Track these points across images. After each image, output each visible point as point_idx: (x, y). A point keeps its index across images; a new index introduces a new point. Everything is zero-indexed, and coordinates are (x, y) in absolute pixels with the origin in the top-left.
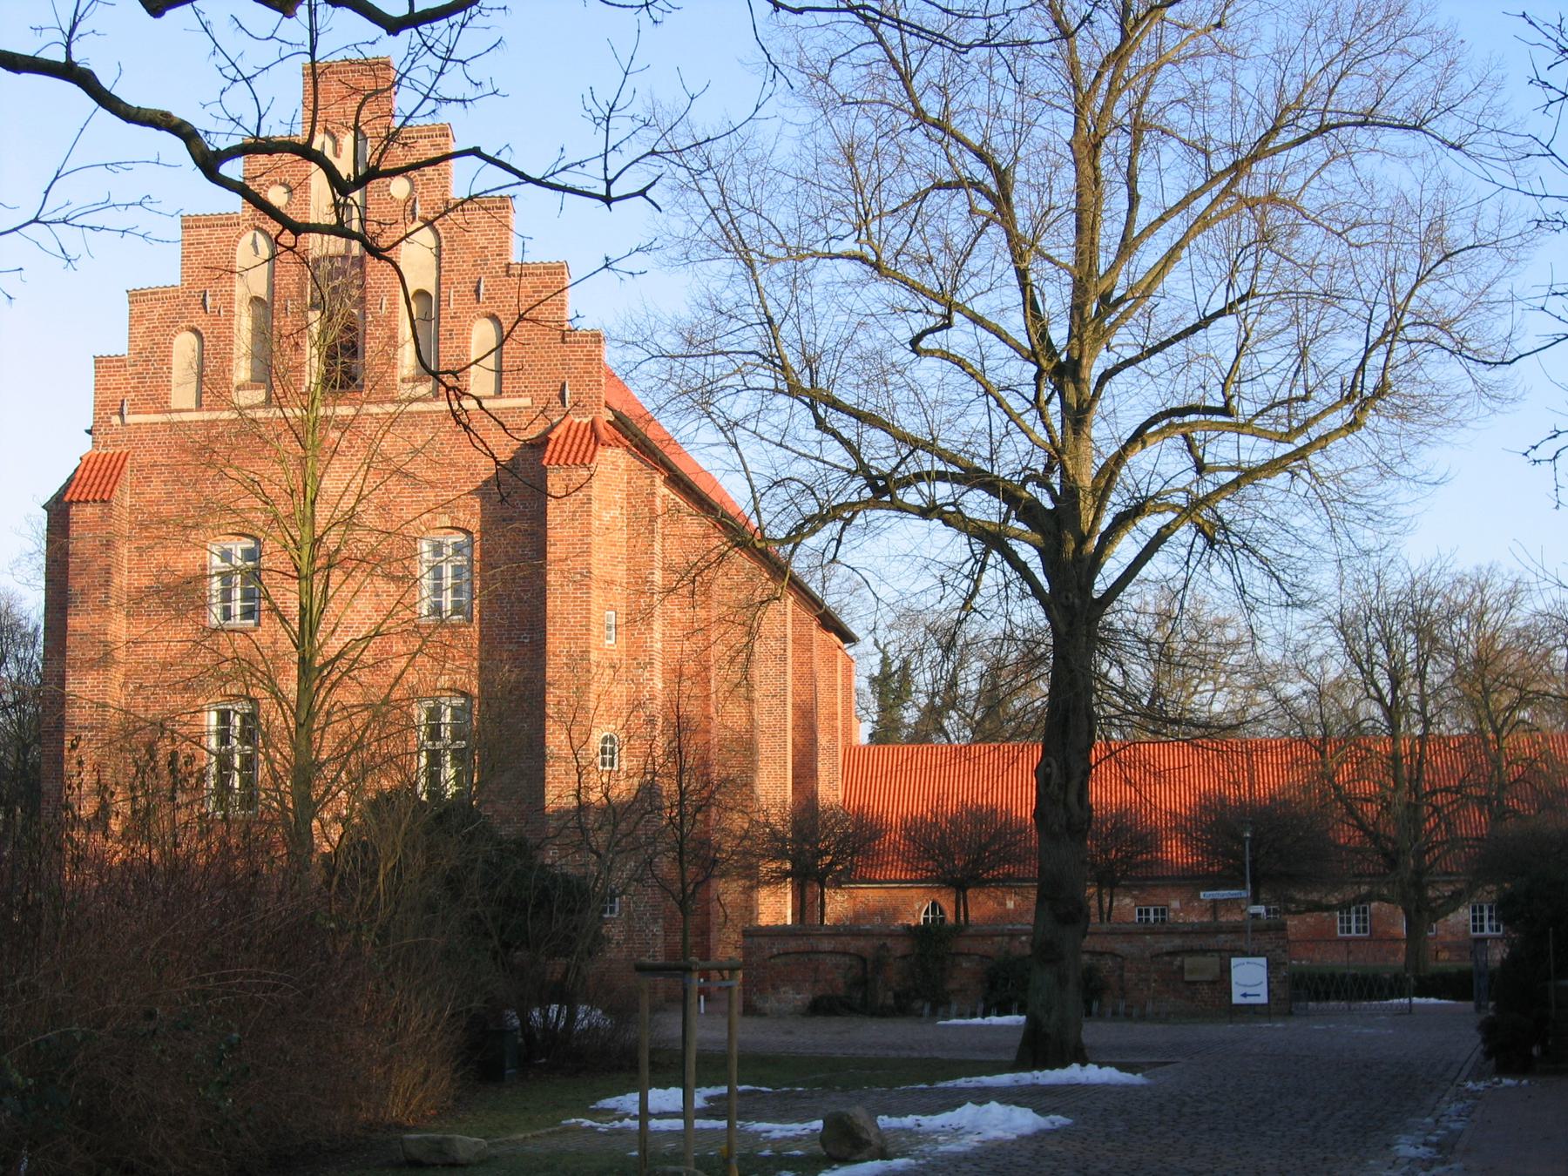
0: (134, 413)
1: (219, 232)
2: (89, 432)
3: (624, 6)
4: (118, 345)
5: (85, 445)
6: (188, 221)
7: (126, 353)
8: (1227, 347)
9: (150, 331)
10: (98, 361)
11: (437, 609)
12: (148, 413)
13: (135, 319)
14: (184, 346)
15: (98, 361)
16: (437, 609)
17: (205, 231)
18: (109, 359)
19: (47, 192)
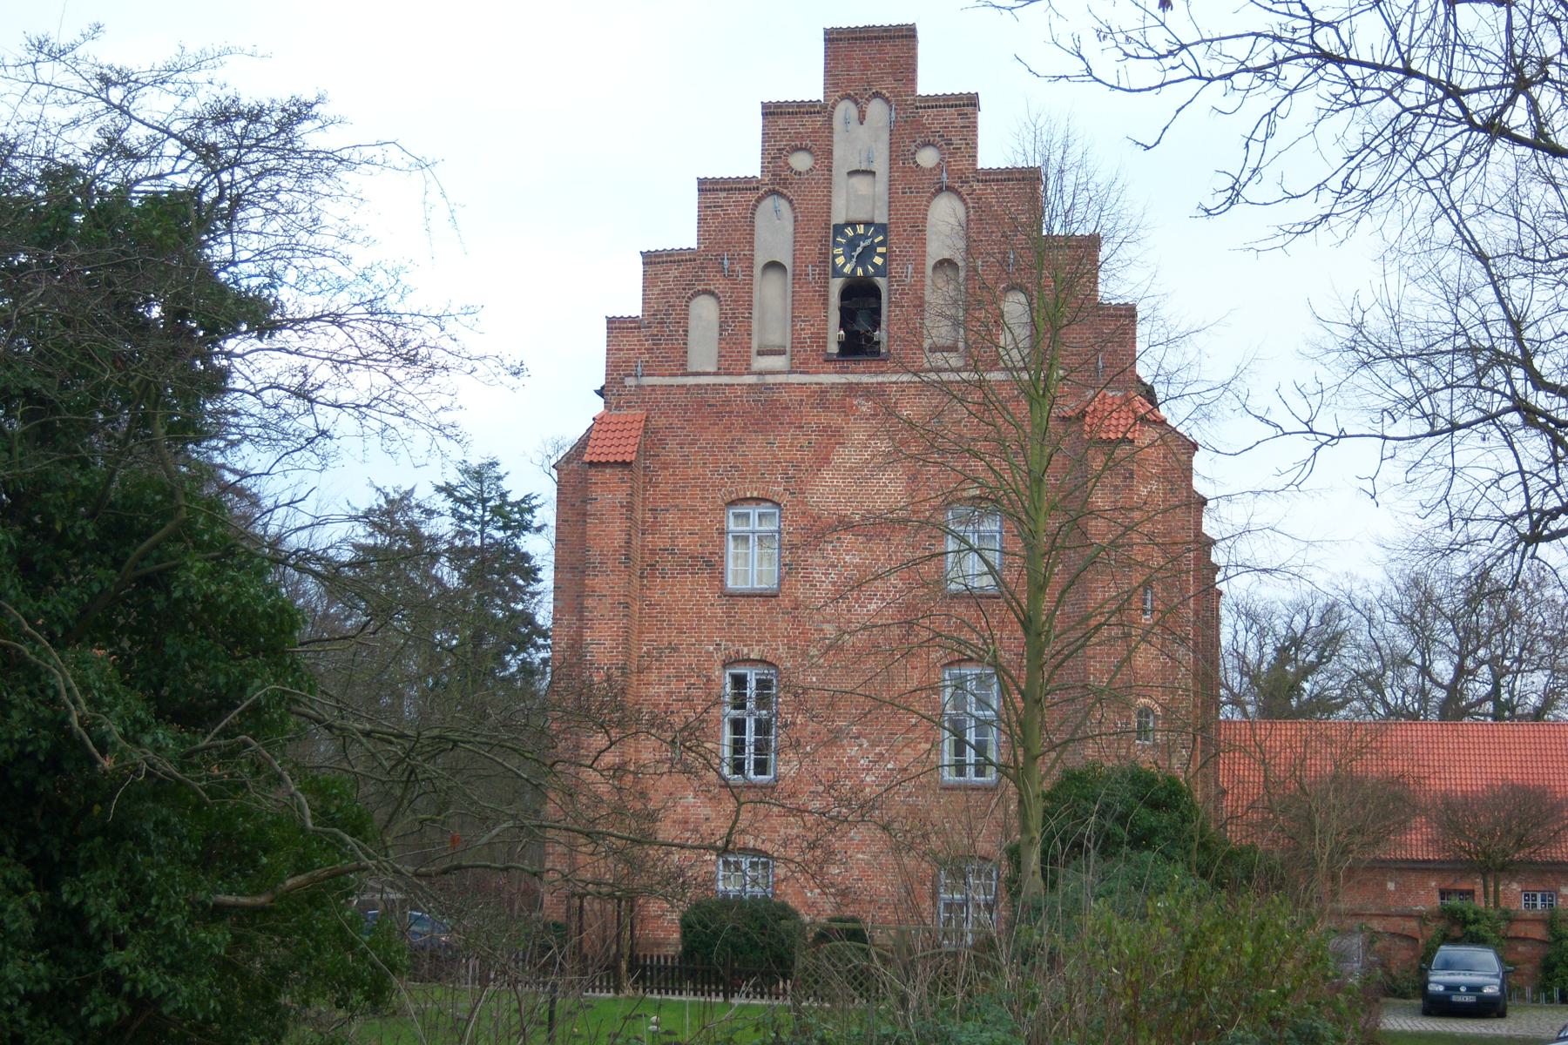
0: (649, 375)
1: (737, 196)
2: (601, 393)
3: (1139, 91)
4: (633, 306)
5: (598, 407)
6: (705, 183)
7: (640, 314)
8: (1379, 209)
9: (665, 293)
10: (611, 321)
11: (785, 982)
12: (663, 376)
13: (649, 282)
14: (705, 312)
15: (611, 321)
16: (785, 982)
17: (723, 195)
18: (622, 320)
19: (1178, 111)
